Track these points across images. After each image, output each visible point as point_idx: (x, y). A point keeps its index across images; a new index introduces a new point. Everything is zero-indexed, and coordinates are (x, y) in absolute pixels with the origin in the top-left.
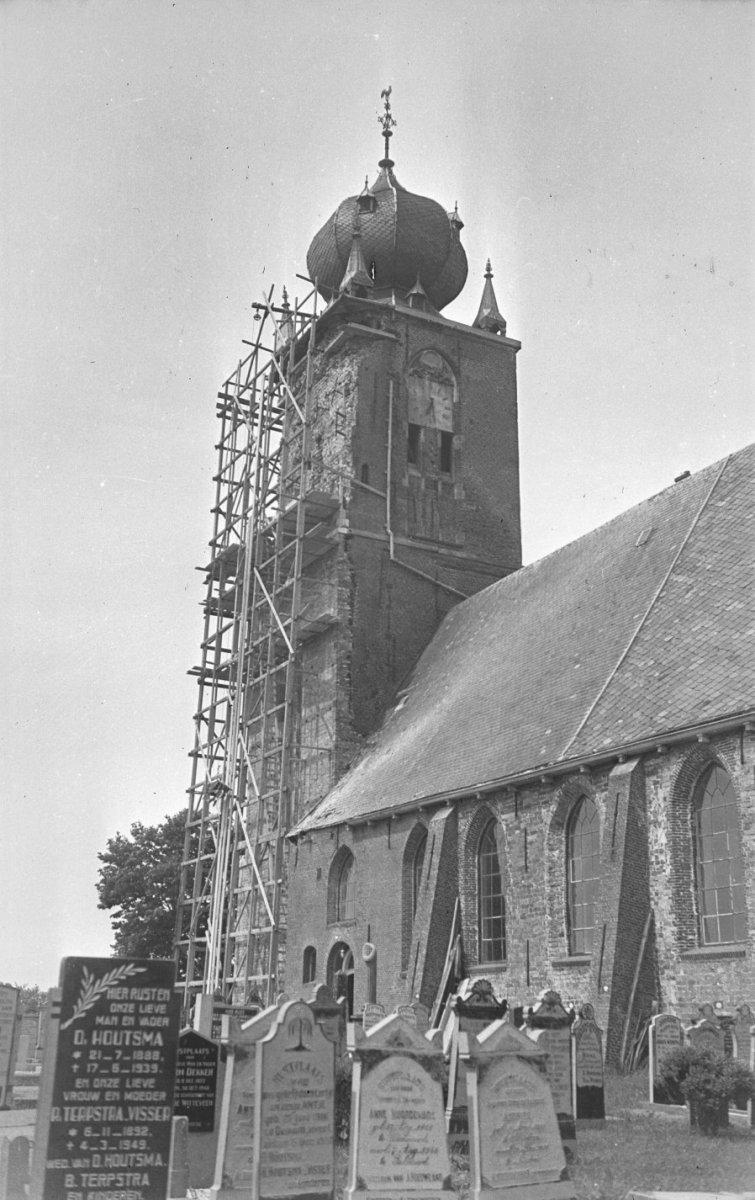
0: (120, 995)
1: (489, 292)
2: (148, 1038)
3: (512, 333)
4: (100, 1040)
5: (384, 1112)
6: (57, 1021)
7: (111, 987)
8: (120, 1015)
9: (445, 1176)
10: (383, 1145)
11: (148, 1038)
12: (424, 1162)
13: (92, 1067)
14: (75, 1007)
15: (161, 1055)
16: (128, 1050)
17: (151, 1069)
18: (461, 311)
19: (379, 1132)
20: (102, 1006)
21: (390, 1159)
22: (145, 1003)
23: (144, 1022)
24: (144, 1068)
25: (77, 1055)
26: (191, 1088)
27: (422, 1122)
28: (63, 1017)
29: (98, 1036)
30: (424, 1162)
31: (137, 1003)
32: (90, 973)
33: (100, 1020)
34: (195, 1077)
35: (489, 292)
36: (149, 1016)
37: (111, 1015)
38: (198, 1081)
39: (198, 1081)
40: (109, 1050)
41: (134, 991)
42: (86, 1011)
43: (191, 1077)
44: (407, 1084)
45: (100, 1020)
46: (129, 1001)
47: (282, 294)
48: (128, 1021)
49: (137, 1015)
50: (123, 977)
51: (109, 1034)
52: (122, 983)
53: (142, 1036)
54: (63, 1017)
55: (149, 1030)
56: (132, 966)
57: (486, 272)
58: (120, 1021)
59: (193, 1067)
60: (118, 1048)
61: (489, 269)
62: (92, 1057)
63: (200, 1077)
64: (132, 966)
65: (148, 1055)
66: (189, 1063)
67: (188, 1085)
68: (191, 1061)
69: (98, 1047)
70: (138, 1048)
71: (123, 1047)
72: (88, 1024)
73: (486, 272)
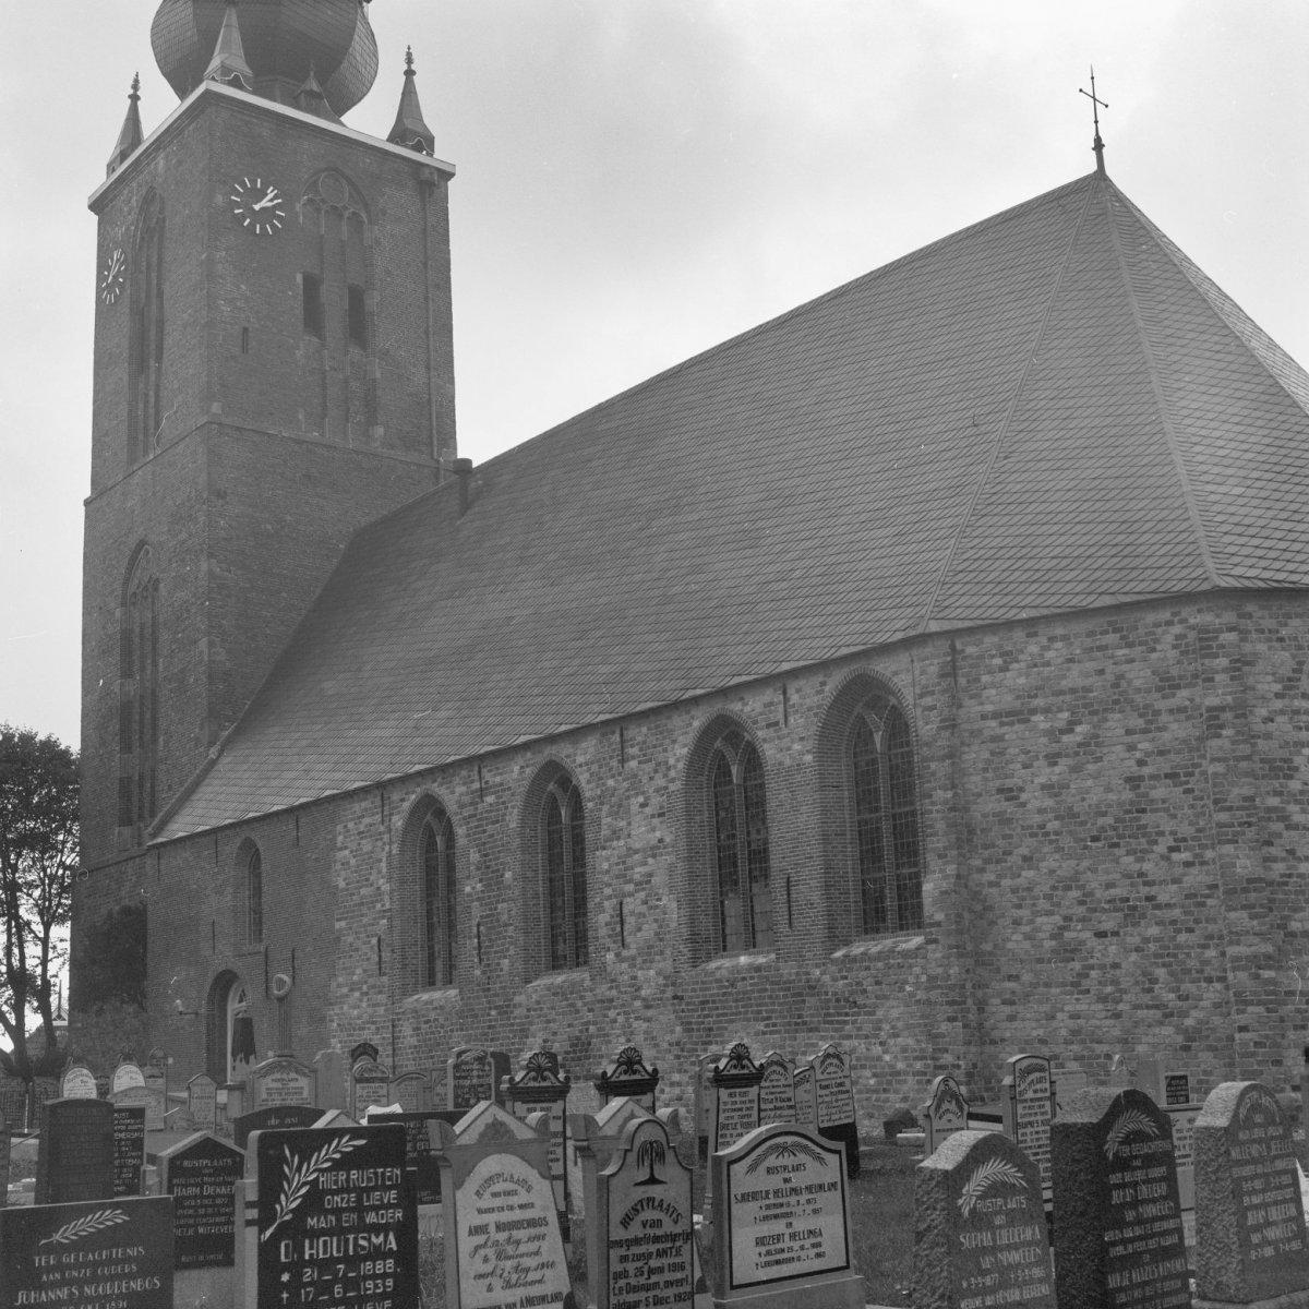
0: (336, 1182)
1: (409, 93)
2: (377, 1240)
3: (443, 153)
4: (314, 1251)
5: (487, 1225)
6: (254, 1230)
7: (322, 1171)
8: (337, 1211)
9: (566, 1290)
10: (488, 1268)
11: (377, 1240)
12: (540, 1281)
13: (307, 1294)
14: (278, 1207)
15: (397, 1264)
16: (352, 1261)
17: (385, 1286)
18: (370, 120)
19: (482, 1252)
20: (314, 1199)
21: (497, 1283)
22: (368, 1190)
23: (371, 1218)
24: (376, 1286)
25: (285, 1277)
26: (210, 1210)
27: (533, 1231)
28: (262, 1224)
29: (311, 1248)
30: (540, 1281)
31: (360, 1191)
32: (293, 1156)
33: (312, 1222)
34: (214, 1197)
35: (409, 93)
36: (376, 1208)
37: (327, 1212)
38: (218, 1201)
39: (218, 1201)
40: (326, 1265)
41: (354, 1174)
42: (292, 1211)
43: (208, 1197)
44: (510, 1186)
45: (312, 1222)
46: (347, 1190)
47: (131, 82)
48: (349, 1219)
49: (360, 1209)
50: (337, 1156)
51: (325, 1242)
52: (337, 1165)
53: (369, 1240)
54: (262, 1224)
55: (376, 1229)
56: (347, 1138)
57: (131, 92)
58: (339, 1220)
59: (211, 1184)
60: (338, 1260)
61: (136, 86)
62: (306, 1279)
63: (219, 1196)
64: (347, 1138)
65: (380, 1267)
66: (206, 1179)
67: (206, 1206)
68: (210, 1175)
69: (313, 1262)
70: (365, 1259)
71: (346, 1259)
72: (295, 1230)
73: (131, 92)
